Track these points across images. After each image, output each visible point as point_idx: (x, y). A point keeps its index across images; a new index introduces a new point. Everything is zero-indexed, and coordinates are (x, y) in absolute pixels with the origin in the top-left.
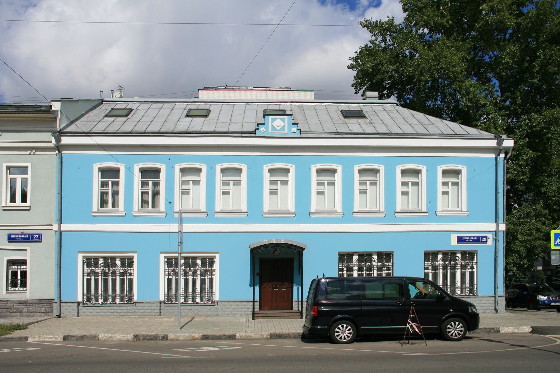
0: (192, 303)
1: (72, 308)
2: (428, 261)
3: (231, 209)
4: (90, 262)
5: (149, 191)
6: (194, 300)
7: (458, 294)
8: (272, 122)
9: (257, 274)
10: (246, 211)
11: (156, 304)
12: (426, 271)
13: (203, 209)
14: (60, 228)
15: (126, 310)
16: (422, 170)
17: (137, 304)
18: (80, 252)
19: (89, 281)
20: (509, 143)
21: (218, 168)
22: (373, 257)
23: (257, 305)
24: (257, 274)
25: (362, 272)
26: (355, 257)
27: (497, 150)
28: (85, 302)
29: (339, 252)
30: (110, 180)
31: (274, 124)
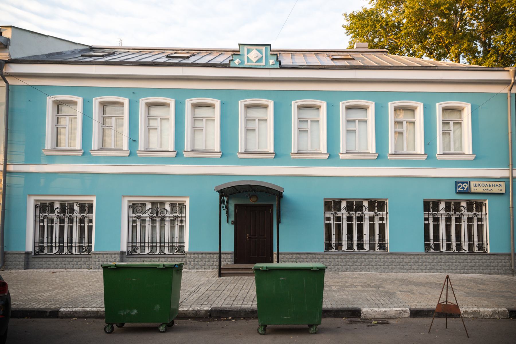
0: (159, 255)
2: (429, 211)
6: (161, 251)
9: (232, 221)
12: (328, 222)
21: (438, 107)
24: (232, 221)
25: (460, 222)
26: (442, 206)
28: (129, 252)
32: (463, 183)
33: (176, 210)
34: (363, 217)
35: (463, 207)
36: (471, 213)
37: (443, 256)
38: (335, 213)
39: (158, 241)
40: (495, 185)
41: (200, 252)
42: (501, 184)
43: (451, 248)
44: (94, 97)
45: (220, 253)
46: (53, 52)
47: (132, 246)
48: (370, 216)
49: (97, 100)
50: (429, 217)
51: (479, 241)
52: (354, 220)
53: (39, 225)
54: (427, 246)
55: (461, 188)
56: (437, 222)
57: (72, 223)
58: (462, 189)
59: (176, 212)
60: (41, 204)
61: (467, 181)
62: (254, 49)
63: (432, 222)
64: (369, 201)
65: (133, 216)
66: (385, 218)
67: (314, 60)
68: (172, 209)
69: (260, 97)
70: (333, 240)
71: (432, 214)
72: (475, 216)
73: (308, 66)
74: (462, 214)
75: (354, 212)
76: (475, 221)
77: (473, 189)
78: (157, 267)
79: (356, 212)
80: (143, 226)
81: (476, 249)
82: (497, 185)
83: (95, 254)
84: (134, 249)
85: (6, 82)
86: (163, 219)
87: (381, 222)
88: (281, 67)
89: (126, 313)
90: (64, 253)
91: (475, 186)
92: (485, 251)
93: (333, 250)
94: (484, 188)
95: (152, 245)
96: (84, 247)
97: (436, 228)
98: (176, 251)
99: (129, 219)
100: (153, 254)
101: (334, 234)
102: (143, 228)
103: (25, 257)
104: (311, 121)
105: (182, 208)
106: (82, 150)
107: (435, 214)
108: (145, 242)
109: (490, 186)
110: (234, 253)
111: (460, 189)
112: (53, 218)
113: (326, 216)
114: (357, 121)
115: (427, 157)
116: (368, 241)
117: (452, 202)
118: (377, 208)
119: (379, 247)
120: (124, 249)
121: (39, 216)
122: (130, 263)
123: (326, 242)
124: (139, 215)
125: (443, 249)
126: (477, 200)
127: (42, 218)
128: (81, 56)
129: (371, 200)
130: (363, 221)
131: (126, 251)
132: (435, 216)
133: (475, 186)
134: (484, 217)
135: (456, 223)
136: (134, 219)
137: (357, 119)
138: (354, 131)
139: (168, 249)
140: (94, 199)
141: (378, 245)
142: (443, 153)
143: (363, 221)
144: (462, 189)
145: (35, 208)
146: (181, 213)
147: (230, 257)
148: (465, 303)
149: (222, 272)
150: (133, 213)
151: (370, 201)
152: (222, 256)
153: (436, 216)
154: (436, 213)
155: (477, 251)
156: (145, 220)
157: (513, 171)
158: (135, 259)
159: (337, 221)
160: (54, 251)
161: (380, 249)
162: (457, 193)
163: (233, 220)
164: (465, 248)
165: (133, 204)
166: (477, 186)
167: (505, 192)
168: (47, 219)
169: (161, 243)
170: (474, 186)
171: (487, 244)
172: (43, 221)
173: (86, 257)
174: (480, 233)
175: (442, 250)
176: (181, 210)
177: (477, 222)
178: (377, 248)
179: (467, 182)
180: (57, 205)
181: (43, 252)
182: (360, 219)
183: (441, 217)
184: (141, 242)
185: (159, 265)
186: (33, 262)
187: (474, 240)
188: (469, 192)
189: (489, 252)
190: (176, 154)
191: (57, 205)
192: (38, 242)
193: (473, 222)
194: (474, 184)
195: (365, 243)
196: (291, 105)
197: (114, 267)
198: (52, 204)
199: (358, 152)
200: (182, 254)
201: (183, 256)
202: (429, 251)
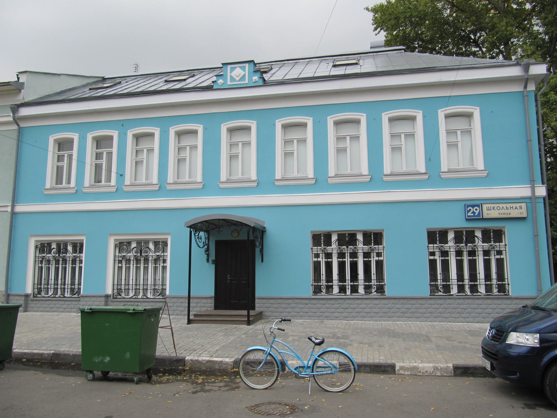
3: (404, 170)
4: (43, 247)
5: (102, 163)
6: (145, 294)
7: (480, 293)
9: (213, 261)
11: (180, 300)
12: (432, 258)
14: (13, 206)
15: (413, 310)
18: (111, 235)
19: (41, 269)
20: (540, 69)
21: (385, 117)
22: (476, 234)
25: (489, 256)
26: (451, 236)
27: (525, 80)
29: (427, 229)
31: (233, 74)
32: (473, 206)
33: (159, 249)
37: (480, 301)
38: (324, 248)
39: (142, 283)
41: (180, 296)
42: (521, 206)
46: (65, 89)
50: (164, 255)
52: (464, 255)
53: (118, 266)
54: (434, 289)
55: (471, 213)
56: (368, 258)
57: (66, 264)
58: (472, 214)
60: (41, 244)
61: (477, 204)
62: (237, 67)
63: (455, 257)
64: (482, 231)
65: (119, 256)
67: (309, 71)
68: (155, 248)
69: (243, 118)
70: (439, 281)
73: (290, 80)
74: (475, 246)
75: (463, 245)
77: (487, 214)
78: (127, 312)
80: (146, 267)
82: (516, 208)
83: (83, 296)
85: (18, 125)
87: (498, 257)
89: (100, 360)
90: (140, 297)
91: (488, 209)
93: (323, 294)
94: (501, 211)
95: (154, 287)
96: (159, 290)
97: (446, 265)
99: (116, 259)
101: (323, 275)
102: (128, 269)
103: (24, 300)
106: (202, 183)
107: (442, 246)
109: (507, 209)
112: (50, 259)
115: (429, 176)
116: (483, 282)
119: (497, 290)
120: (109, 291)
122: (115, 307)
123: (431, 283)
124: (123, 254)
125: (454, 290)
127: (120, 259)
128: (89, 89)
129: (365, 232)
131: (111, 295)
133: (488, 209)
135: (364, 259)
138: (344, 150)
140: (84, 238)
141: (496, 287)
142: (448, 170)
143: (370, 258)
144: (472, 214)
145: (35, 248)
146: (163, 252)
147: (209, 302)
150: (119, 252)
151: (484, 230)
154: (458, 245)
155: (497, 294)
156: (130, 260)
157: (536, 189)
158: (119, 303)
160: (50, 294)
161: (499, 292)
162: (467, 220)
163: (214, 258)
165: (120, 243)
166: (491, 210)
167: (526, 216)
170: (487, 210)
172: (120, 262)
173: (75, 301)
178: (495, 290)
179: (478, 206)
180: (54, 246)
181: (40, 294)
182: (472, 253)
183: (346, 252)
184: (144, 284)
185: (129, 310)
186: (32, 304)
188: (481, 217)
190: (159, 187)
191: (54, 246)
192: (116, 284)
194: (487, 207)
195: (480, 285)
196: (274, 125)
197: (132, 311)
198: (49, 244)
200: (163, 298)
201: (164, 300)
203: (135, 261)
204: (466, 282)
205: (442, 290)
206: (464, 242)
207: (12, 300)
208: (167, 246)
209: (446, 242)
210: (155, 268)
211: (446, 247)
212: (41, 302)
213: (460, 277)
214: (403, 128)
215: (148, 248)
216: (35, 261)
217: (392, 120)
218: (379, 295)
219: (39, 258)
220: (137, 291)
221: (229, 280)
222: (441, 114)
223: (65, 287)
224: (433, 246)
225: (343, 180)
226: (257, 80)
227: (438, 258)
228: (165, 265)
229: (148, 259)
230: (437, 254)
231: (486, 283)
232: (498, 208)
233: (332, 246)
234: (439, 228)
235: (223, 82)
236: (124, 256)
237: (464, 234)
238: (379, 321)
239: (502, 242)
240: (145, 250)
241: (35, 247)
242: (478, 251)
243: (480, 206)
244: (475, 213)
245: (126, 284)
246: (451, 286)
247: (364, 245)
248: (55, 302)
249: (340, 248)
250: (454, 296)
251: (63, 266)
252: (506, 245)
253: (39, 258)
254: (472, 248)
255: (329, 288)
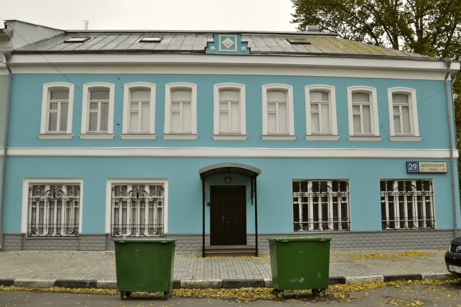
1: (15, 241)
2: (385, 190)
3: (181, 131)
6: (142, 233)
8: (222, 41)
9: (208, 203)
10: (196, 133)
11: (101, 238)
12: (295, 203)
13: (152, 131)
16: (331, 91)
17: (82, 238)
18: (25, 178)
22: (328, 185)
23: (208, 240)
24: (208, 203)
25: (411, 201)
26: (396, 185)
30: (361, 104)
31: (224, 42)
32: (413, 163)
33: (72, 192)
34: (328, 197)
35: (413, 186)
36: (420, 192)
39: (55, 222)
40: (439, 165)
43: (404, 225)
44: (126, 83)
45: (256, 235)
47: (32, 228)
48: (334, 196)
49: (308, 88)
50: (161, 198)
51: (427, 218)
54: (384, 224)
56: (325, 202)
58: (412, 169)
59: (154, 194)
61: (416, 161)
63: (312, 202)
65: (33, 198)
66: (347, 198)
68: (68, 192)
71: (387, 193)
72: (423, 195)
74: (412, 193)
75: (319, 192)
76: (424, 198)
79: (321, 193)
80: (41, 208)
81: (425, 226)
84: (116, 231)
85: (10, 71)
86: (60, 200)
87: (343, 202)
88: (252, 54)
92: (433, 227)
97: (391, 206)
98: (71, 233)
100: (134, 237)
104: (279, 104)
105: (161, 190)
108: (61, 224)
110: (210, 235)
111: (410, 169)
113: (294, 197)
114: (229, 103)
116: (332, 221)
117: (404, 181)
118: (339, 189)
121: (32, 199)
125: (398, 226)
126: (424, 179)
127: (34, 201)
128: (63, 42)
130: (307, 202)
132: (390, 195)
134: (430, 195)
136: (117, 201)
137: (320, 102)
139: (64, 231)
144: (412, 169)
146: (76, 195)
148: (399, 284)
149: (206, 253)
150: (33, 195)
152: (259, 237)
153: (391, 195)
154: (391, 192)
155: (426, 228)
159: (304, 202)
161: (343, 228)
163: (209, 201)
164: (416, 224)
165: (34, 186)
168: (39, 201)
169: (141, 225)
171: (434, 221)
172: (34, 203)
174: (428, 210)
175: (396, 228)
176: (160, 192)
177: (425, 200)
178: (340, 227)
179: (415, 163)
182: (325, 199)
183: (395, 196)
187: (423, 217)
188: (418, 172)
189: (436, 228)
193: (422, 200)
195: (330, 223)
196: (261, 89)
199: (322, 134)
201: (77, 238)
202: (386, 229)
203: (48, 203)
204: (406, 219)
205: (302, 228)
206: (319, 190)
207: (7, 240)
208: (79, 189)
209: (306, 191)
210: (68, 210)
211: (306, 194)
212: (38, 241)
213: (402, 216)
214: (182, 97)
215: (61, 191)
216: (29, 202)
217: (221, 90)
218: (344, 231)
219: (33, 200)
220: (133, 230)
221: (224, 219)
222: (307, 90)
223: (140, 227)
224: (384, 193)
225: (170, 138)
226: (245, 50)
227: (387, 201)
228: (77, 207)
229: (61, 201)
230: (300, 200)
231: (409, 220)
232: (429, 165)
233: (308, 191)
234: (301, 179)
235: (214, 48)
236: (38, 198)
237: (320, 184)
238: (353, 250)
239: (346, 191)
240: (58, 193)
241: (29, 189)
242: (309, 197)
243: (417, 163)
244: (414, 168)
245: (58, 223)
246: (309, 224)
247: (333, 191)
248: (52, 240)
249: (315, 193)
250: (398, 230)
251: (58, 207)
252: (349, 193)
253: (33, 200)
254: (325, 195)
255: (306, 226)
